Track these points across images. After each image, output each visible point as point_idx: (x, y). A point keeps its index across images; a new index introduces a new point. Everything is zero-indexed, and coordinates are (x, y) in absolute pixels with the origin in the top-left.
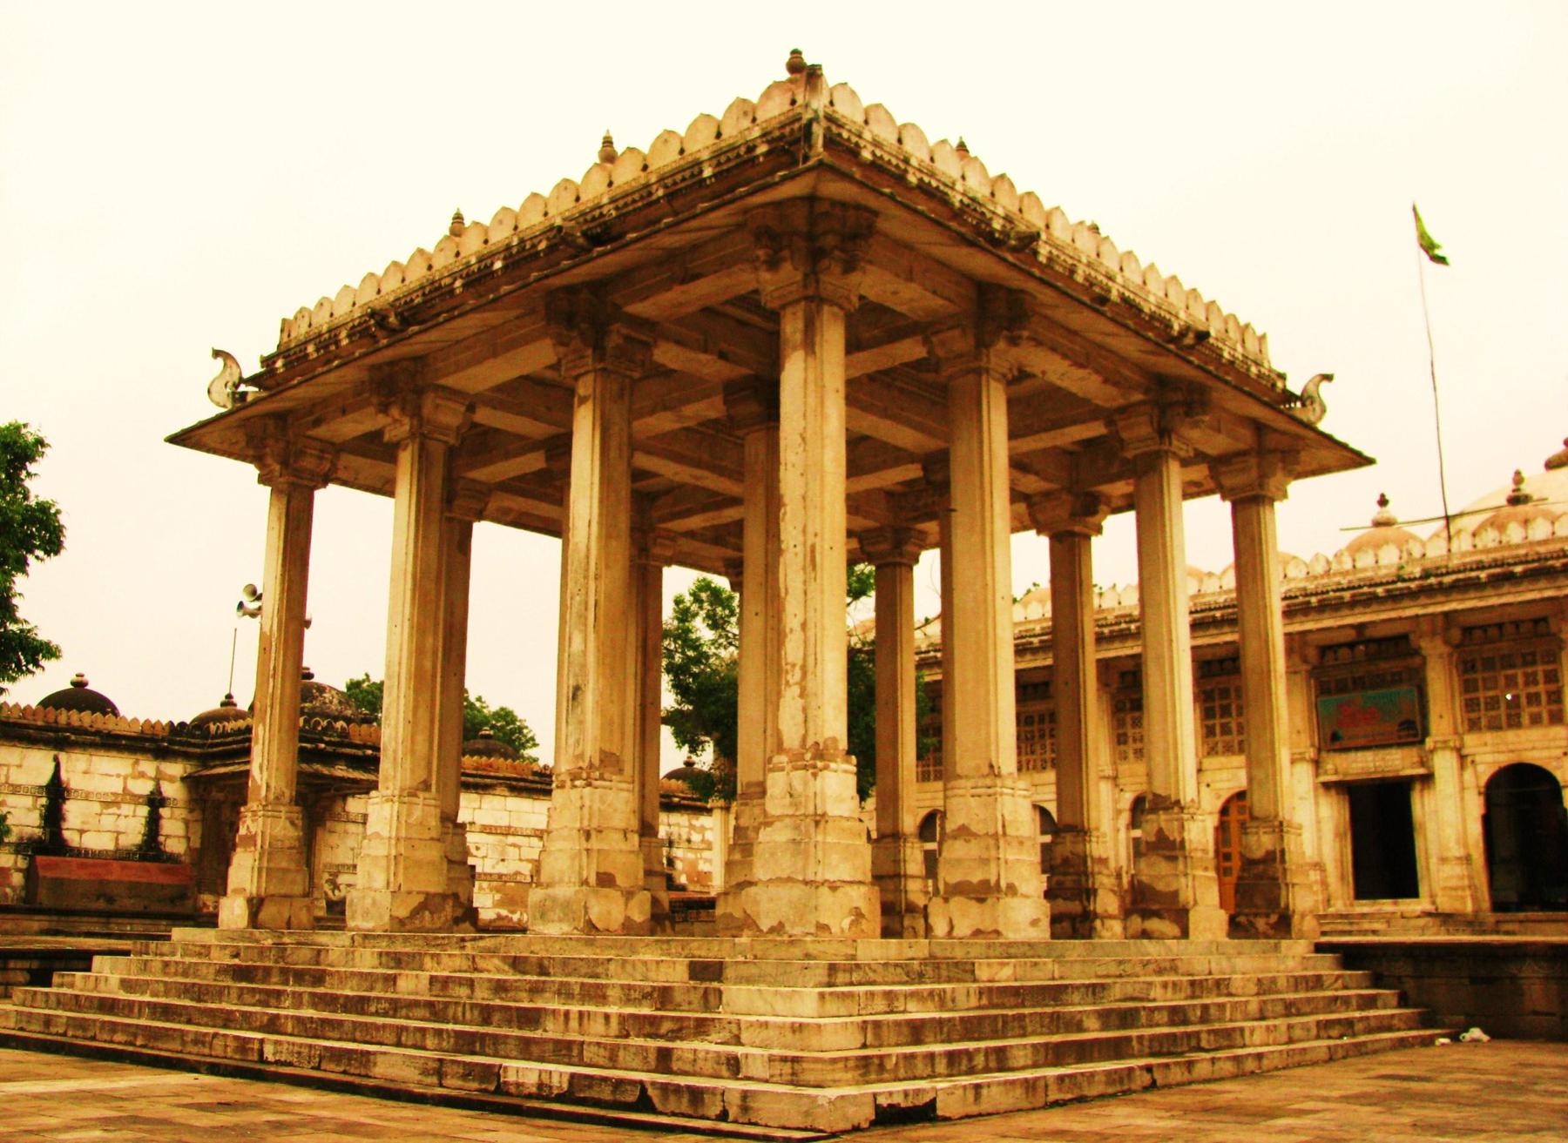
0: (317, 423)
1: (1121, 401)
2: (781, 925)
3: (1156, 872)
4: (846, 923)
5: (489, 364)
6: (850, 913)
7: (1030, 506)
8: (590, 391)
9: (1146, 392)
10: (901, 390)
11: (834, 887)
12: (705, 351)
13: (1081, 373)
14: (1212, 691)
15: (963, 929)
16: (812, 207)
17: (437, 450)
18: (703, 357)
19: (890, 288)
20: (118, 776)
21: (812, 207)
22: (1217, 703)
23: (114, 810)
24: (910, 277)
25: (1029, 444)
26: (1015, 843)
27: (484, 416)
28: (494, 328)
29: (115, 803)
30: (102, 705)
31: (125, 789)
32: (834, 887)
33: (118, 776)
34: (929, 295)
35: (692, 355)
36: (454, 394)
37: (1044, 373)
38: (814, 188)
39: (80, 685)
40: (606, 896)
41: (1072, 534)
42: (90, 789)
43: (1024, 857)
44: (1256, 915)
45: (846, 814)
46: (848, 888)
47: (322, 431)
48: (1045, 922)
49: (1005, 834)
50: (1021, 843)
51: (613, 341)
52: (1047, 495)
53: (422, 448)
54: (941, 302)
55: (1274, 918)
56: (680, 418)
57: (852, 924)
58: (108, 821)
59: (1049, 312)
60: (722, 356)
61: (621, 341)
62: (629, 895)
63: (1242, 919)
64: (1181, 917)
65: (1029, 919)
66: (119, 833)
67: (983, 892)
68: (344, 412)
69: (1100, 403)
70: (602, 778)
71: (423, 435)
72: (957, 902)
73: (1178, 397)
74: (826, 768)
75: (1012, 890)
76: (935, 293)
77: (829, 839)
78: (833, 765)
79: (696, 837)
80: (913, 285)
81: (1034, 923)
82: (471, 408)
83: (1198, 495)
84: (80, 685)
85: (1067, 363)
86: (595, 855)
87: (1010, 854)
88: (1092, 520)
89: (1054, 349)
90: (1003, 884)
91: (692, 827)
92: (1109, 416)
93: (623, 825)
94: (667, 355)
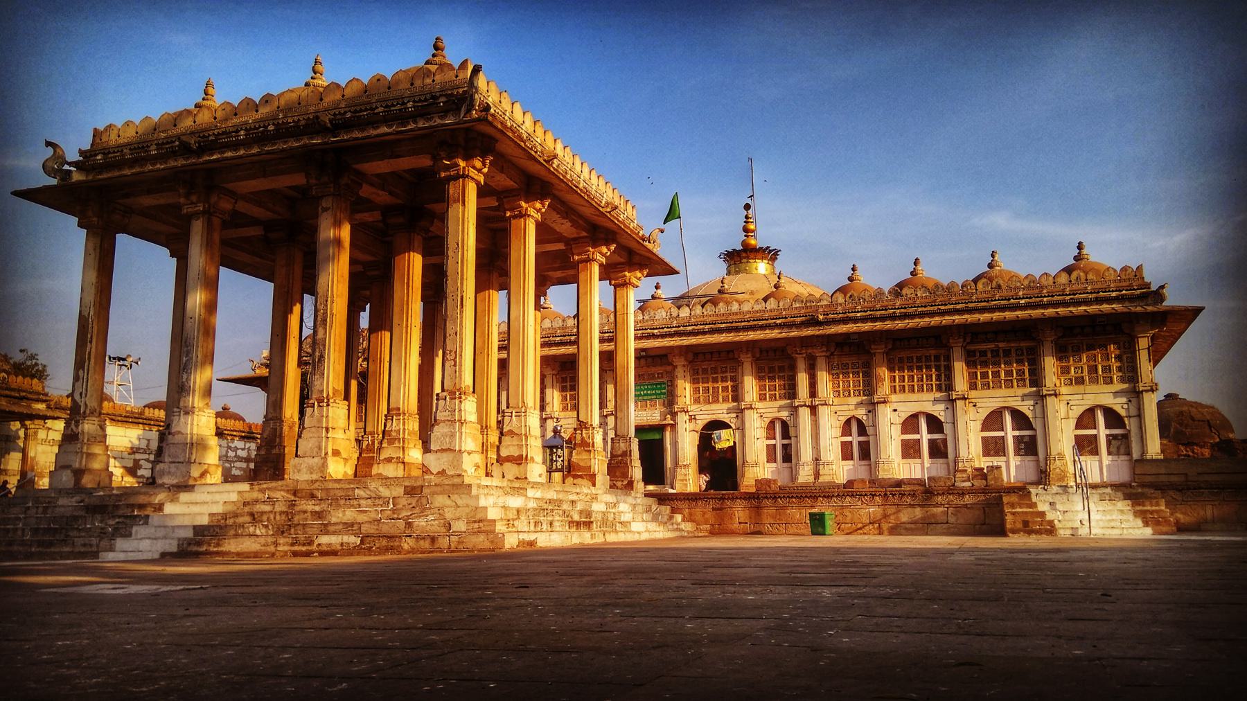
35: (374, 190)
62: (346, 460)
79: (231, 454)
87: (531, 441)
91: (229, 447)
92: (569, 242)
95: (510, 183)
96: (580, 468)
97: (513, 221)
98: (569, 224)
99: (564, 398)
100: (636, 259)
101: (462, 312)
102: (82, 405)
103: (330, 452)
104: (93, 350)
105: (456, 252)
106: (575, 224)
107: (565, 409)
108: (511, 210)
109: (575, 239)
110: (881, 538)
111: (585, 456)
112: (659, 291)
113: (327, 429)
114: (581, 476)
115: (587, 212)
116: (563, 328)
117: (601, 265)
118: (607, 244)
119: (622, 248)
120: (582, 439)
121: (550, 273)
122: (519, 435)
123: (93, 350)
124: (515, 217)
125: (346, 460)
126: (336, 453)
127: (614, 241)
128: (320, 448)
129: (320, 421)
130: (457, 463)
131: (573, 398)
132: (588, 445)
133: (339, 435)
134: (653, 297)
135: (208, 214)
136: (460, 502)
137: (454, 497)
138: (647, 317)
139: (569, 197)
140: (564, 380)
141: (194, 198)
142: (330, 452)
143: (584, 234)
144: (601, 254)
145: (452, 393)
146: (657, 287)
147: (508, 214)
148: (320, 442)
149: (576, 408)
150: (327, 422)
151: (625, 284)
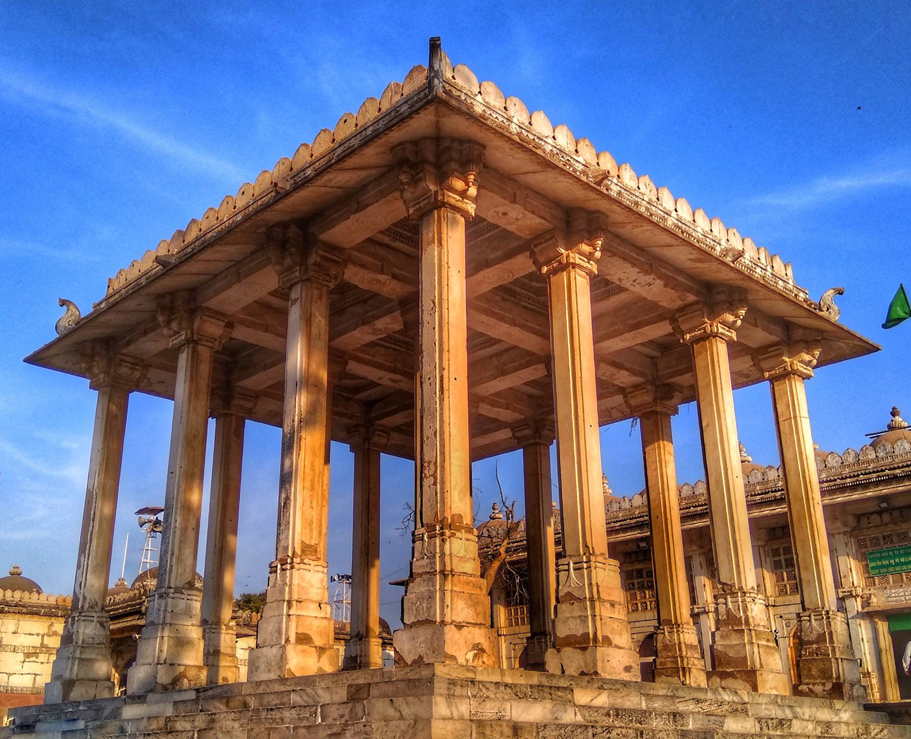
0: (129, 343)
1: (679, 303)
2: (421, 657)
3: (726, 643)
4: (470, 656)
5: (237, 287)
6: (473, 648)
7: (625, 396)
8: (298, 295)
9: (697, 294)
10: (525, 308)
11: (459, 627)
12: (382, 273)
13: (649, 278)
14: (778, 549)
15: (572, 670)
16: (438, 146)
17: (205, 352)
18: (382, 277)
19: (501, 209)
20: (38, 635)
21: (438, 146)
22: (782, 558)
23: (34, 659)
24: (514, 201)
25: (616, 344)
26: (608, 605)
27: (242, 334)
28: (239, 262)
29: (35, 654)
30: (31, 587)
31: (42, 644)
32: (459, 627)
33: (38, 635)
34: (529, 215)
35: (372, 275)
36: (218, 314)
37: (620, 280)
38: (437, 126)
39: (15, 574)
40: (304, 651)
41: (655, 413)
42: (17, 644)
43: (616, 616)
44: (814, 684)
45: (470, 572)
46: (471, 628)
47: (131, 349)
48: (637, 670)
49: (599, 597)
50: (613, 605)
51: (313, 259)
52: (636, 387)
53: (194, 351)
54: (538, 220)
55: (829, 686)
56: (375, 331)
57: (475, 656)
58: (30, 667)
59: (620, 231)
60: (395, 277)
61: (318, 259)
62: (321, 650)
63: (804, 688)
64: (751, 677)
65: (622, 666)
66: (36, 675)
67: (583, 643)
68: (145, 333)
69: (665, 304)
70: (302, 562)
71: (194, 341)
72: (568, 651)
73: (722, 297)
74: (453, 535)
75: (607, 641)
76: (533, 213)
77: (455, 589)
78: (458, 534)
80: (517, 206)
81: (628, 669)
82: (230, 325)
83: (746, 384)
84: (15, 574)
85: (637, 270)
86: (293, 618)
87: (604, 611)
88: (669, 403)
89: (625, 258)
90: (600, 637)
92: (673, 316)
93: (318, 598)
94: (354, 275)
95: (534, 221)
96: (729, 662)
97: (553, 279)
98: (659, 283)
99: (780, 578)
100: (798, 334)
101: (442, 400)
102: (81, 597)
103: (293, 638)
104: (96, 529)
105: (432, 315)
106: (669, 282)
107: (782, 592)
108: (548, 262)
109: (681, 310)
110: (817, 495)
111: (734, 640)
112: (898, 419)
113: (289, 603)
114: (732, 675)
115: (680, 256)
116: (764, 482)
117: (730, 344)
118: (732, 310)
119: (757, 316)
120: (728, 611)
121: (677, 379)
122: (582, 600)
123: (96, 529)
124: (555, 272)
125: (321, 650)
126: (304, 639)
127: (743, 302)
128: (279, 632)
129: (282, 592)
130: (437, 646)
131: (792, 577)
132: (738, 621)
133: (311, 611)
134: (891, 428)
135: (192, 342)
136: (406, 711)
137: (399, 701)
138: (881, 454)
139: (642, 234)
140: (776, 553)
141: (174, 326)
142: (293, 638)
143: (691, 298)
144: (726, 326)
145: (431, 528)
146: (894, 413)
147: (545, 269)
148: (280, 623)
149: (797, 588)
150: (290, 593)
151: (787, 375)
